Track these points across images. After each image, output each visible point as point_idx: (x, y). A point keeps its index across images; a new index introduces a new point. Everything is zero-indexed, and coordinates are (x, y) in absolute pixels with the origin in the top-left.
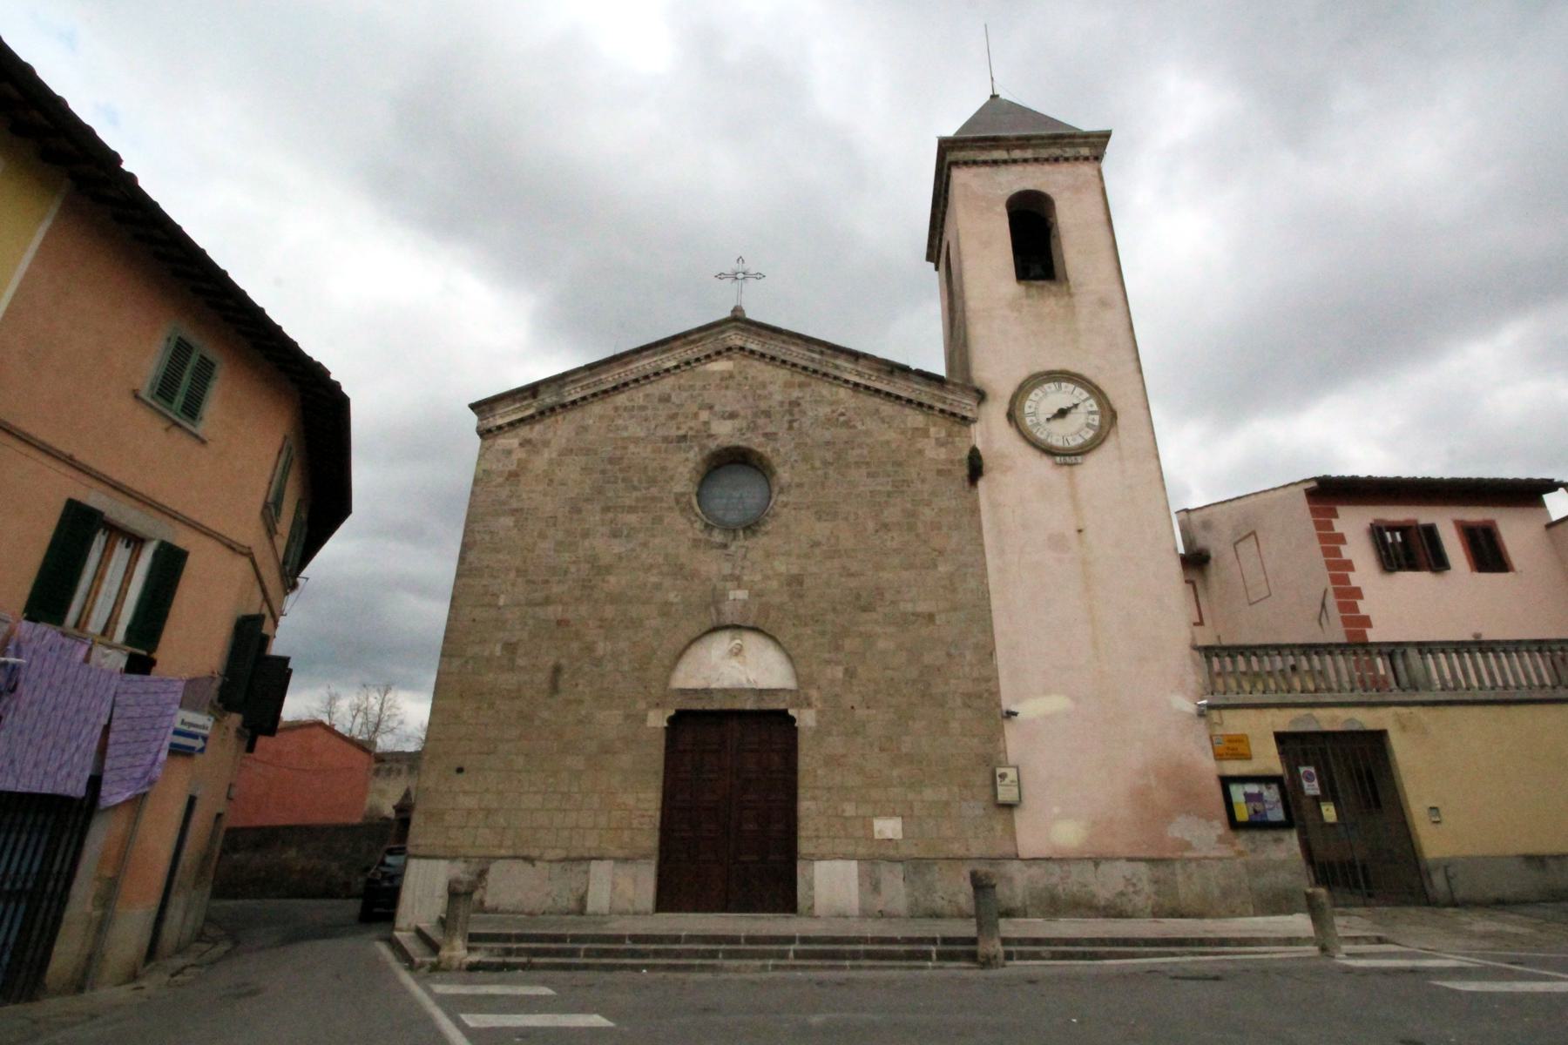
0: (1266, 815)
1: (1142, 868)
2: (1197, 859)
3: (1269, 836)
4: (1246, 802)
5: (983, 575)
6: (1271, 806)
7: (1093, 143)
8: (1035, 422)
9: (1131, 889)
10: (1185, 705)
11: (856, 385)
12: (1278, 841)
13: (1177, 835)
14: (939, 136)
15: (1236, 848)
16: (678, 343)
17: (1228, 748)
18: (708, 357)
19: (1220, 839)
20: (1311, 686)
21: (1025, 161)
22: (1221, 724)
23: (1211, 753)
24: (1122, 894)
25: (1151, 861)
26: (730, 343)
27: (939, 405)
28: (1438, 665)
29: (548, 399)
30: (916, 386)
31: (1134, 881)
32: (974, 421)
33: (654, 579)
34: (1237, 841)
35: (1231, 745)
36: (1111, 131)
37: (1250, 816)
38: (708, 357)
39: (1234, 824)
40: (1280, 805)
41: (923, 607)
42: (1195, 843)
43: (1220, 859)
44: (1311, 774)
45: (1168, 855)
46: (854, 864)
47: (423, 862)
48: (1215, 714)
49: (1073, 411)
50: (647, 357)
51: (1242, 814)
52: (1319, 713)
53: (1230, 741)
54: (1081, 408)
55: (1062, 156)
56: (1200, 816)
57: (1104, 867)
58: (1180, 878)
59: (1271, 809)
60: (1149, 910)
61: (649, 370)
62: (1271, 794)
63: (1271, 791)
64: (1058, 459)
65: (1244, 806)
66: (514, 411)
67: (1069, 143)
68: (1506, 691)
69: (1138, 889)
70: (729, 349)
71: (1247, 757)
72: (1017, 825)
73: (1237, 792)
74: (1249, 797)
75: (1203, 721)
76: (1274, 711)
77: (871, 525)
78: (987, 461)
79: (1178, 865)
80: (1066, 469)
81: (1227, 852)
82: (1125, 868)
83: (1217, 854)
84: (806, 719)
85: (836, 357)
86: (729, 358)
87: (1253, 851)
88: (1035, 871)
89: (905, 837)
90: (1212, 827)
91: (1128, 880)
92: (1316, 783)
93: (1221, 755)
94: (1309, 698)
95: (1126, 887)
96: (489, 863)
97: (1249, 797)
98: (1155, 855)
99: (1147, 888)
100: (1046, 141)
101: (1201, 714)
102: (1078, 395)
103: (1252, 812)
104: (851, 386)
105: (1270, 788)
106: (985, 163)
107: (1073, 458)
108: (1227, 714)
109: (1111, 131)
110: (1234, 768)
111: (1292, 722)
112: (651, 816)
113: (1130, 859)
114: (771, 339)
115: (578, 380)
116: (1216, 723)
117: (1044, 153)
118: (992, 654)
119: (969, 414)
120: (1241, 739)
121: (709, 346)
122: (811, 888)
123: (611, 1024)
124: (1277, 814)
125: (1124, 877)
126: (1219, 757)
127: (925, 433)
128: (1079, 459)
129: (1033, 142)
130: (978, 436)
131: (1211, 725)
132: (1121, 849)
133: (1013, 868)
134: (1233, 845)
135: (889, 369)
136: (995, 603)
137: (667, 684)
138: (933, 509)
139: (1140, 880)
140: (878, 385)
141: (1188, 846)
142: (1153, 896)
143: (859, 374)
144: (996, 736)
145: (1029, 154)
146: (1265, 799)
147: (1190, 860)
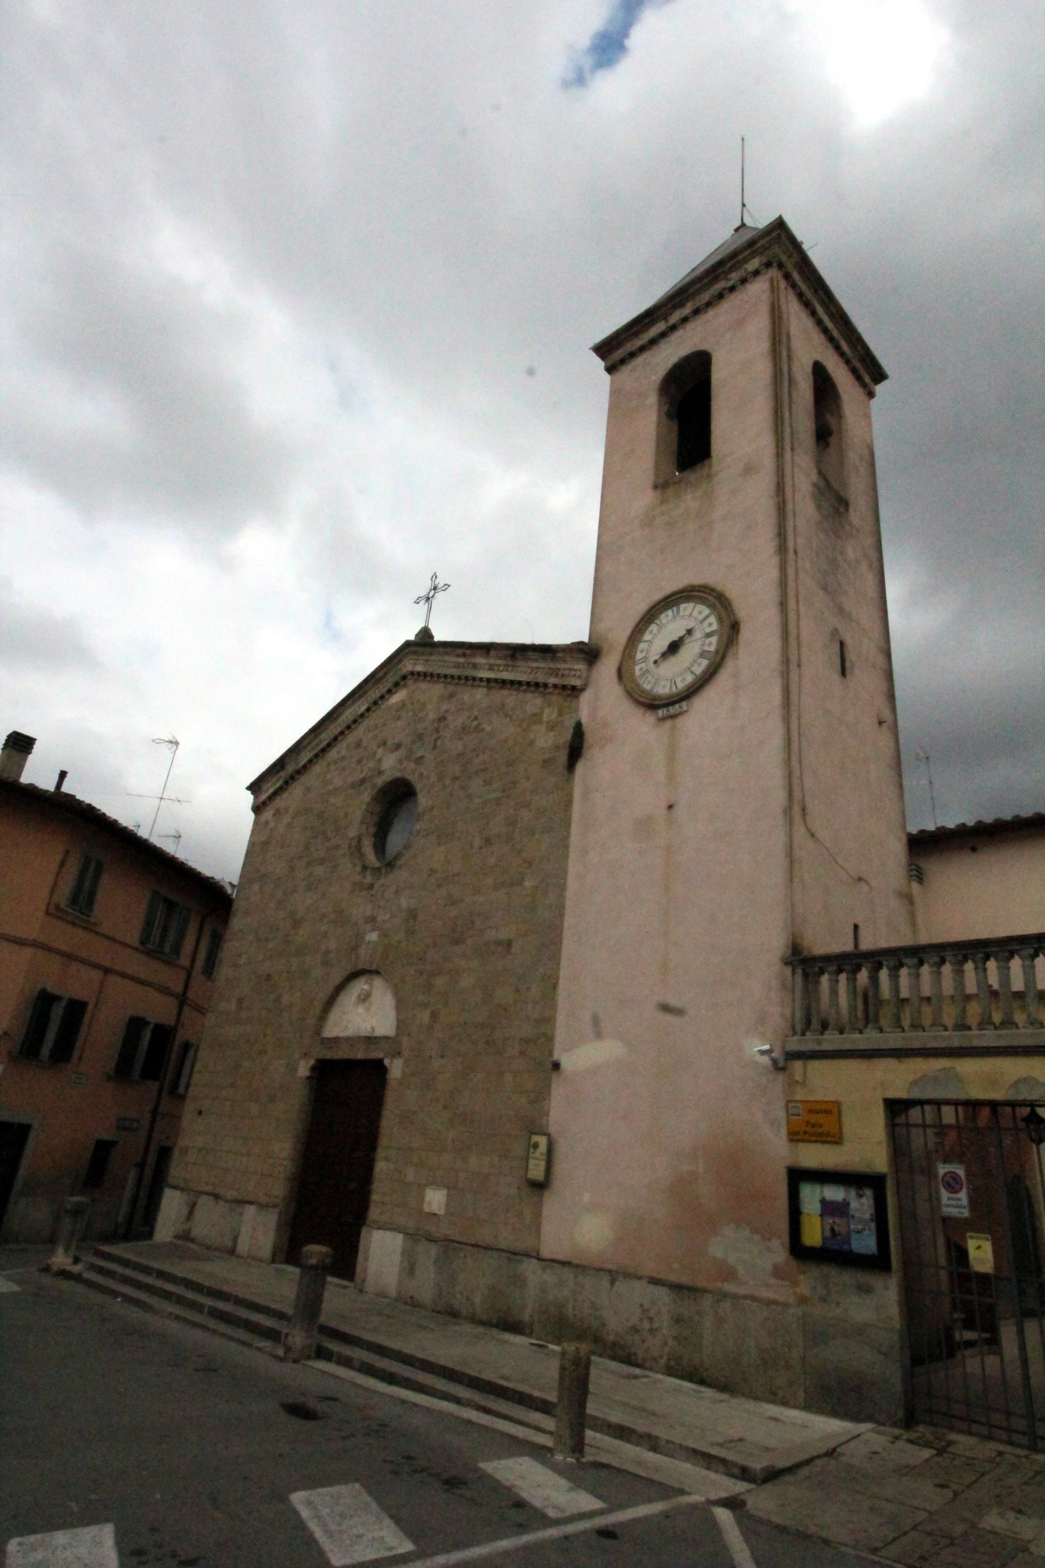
0: (848, 1241)
1: (662, 1292)
2: (735, 1297)
3: (848, 1277)
4: (821, 1216)
5: (563, 887)
6: (860, 1227)
7: (762, 246)
8: (645, 669)
9: (646, 1325)
10: (756, 1047)
11: (489, 680)
12: (865, 1289)
13: (719, 1255)
14: (592, 345)
15: (798, 1290)
16: (370, 685)
17: (808, 1123)
18: (389, 691)
19: (777, 1272)
20: (997, 1018)
21: (685, 320)
22: (803, 1084)
23: (784, 1131)
24: (635, 1330)
25: (677, 1288)
26: (404, 671)
27: (552, 680)
28: (834, 992)
29: (290, 769)
30: (535, 665)
31: (652, 1314)
32: (582, 690)
33: (324, 928)
34: (802, 1277)
35: (814, 1119)
36: (780, 217)
37: (824, 1238)
38: (389, 691)
39: (798, 1250)
40: (873, 1225)
41: (504, 934)
42: (741, 1271)
43: (769, 1303)
44: (954, 1176)
45: (701, 1283)
46: (401, 1236)
47: (172, 1190)
48: (798, 1065)
49: (687, 640)
50: (349, 707)
51: (813, 1235)
52: (967, 1067)
53: (811, 1111)
54: (698, 634)
55: (724, 289)
56: (754, 1230)
57: (621, 1286)
58: (708, 1323)
59: (858, 1232)
60: (663, 1361)
61: (351, 718)
62: (862, 1205)
63: (864, 1200)
64: (661, 713)
65: (817, 1221)
66: (274, 784)
67: (733, 266)
68: (803, 1038)
69: (655, 1326)
70: (404, 678)
71: (835, 1139)
72: (546, 1211)
73: (811, 1196)
74: (829, 1208)
75: (781, 1077)
76: (891, 1063)
77: (477, 842)
78: (589, 737)
79: (707, 1302)
80: (668, 724)
81: (779, 1292)
82: (639, 1293)
83: (771, 1295)
84: (396, 1069)
85: (473, 655)
86: (405, 686)
87: (823, 1299)
88: (549, 1277)
89: (447, 1213)
90: (769, 1249)
91: (645, 1311)
92: (963, 1195)
93: (797, 1133)
94: (956, 1039)
95: (641, 1320)
96: (198, 1197)
97: (829, 1208)
98: (685, 1280)
99: (664, 1323)
100: (705, 281)
101: (778, 1068)
102: (651, 636)
103: (828, 1233)
104: (485, 684)
105: (861, 1196)
106: (642, 349)
107: (677, 706)
108: (816, 1066)
109: (780, 217)
110: (814, 1156)
111: (915, 1083)
112: (285, 1166)
113: (655, 1281)
114: (431, 654)
115: (309, 744)
116: (797, 1082)
117: (706, 297)
118: (555, 987)
119: (577, 683)
120: (832, 1110)
121: (392, 678)
122: (366, 1259)
123: (16, 1288)
124: (866, 1243)
125: (642, 1306)
126: (795, 1137)
127: (536, 718)
128: (684, 704)
129: (691, 291)
130: (585, 708)
131: (791, 1084)
132: (649, 1267)
133: (530, 1268)
134: (795, 1284)
135: (509, 653)
136: (568, 921)
137: (318, 1032)
138: (532, 810)
139: (659, 1313)
140: (506, 675)
141: (728, 1273)
142: (670, 1341)
143: (491, 668)
144: (541, 1095)
145: (687, 310)
146: (852, 1212)
147: (725, 1295)
